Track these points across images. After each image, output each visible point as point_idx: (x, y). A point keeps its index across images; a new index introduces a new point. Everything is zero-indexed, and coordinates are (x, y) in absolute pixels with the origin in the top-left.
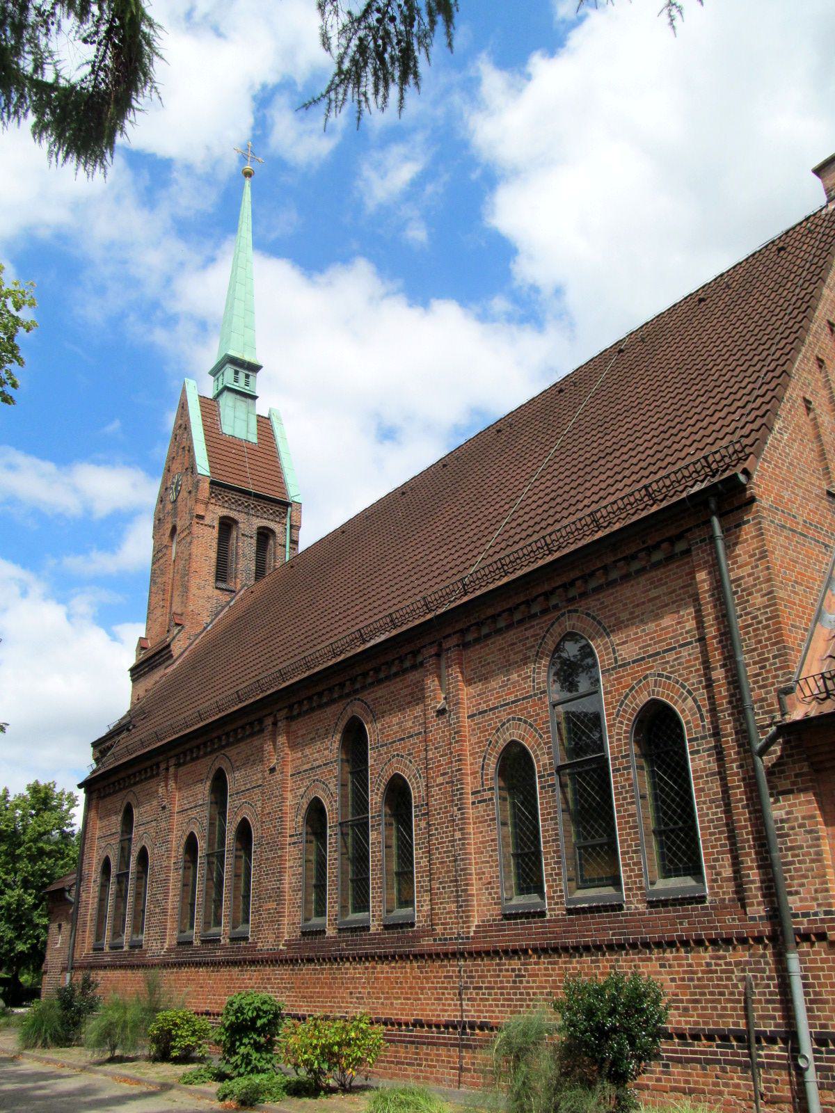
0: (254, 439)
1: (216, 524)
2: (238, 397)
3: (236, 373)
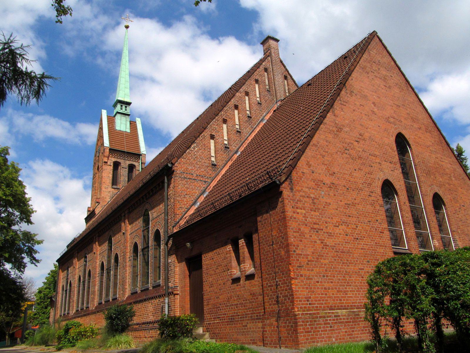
0: (128, 131)
1: (112, 164)
2: (122, 115)
3: (122, 106)
